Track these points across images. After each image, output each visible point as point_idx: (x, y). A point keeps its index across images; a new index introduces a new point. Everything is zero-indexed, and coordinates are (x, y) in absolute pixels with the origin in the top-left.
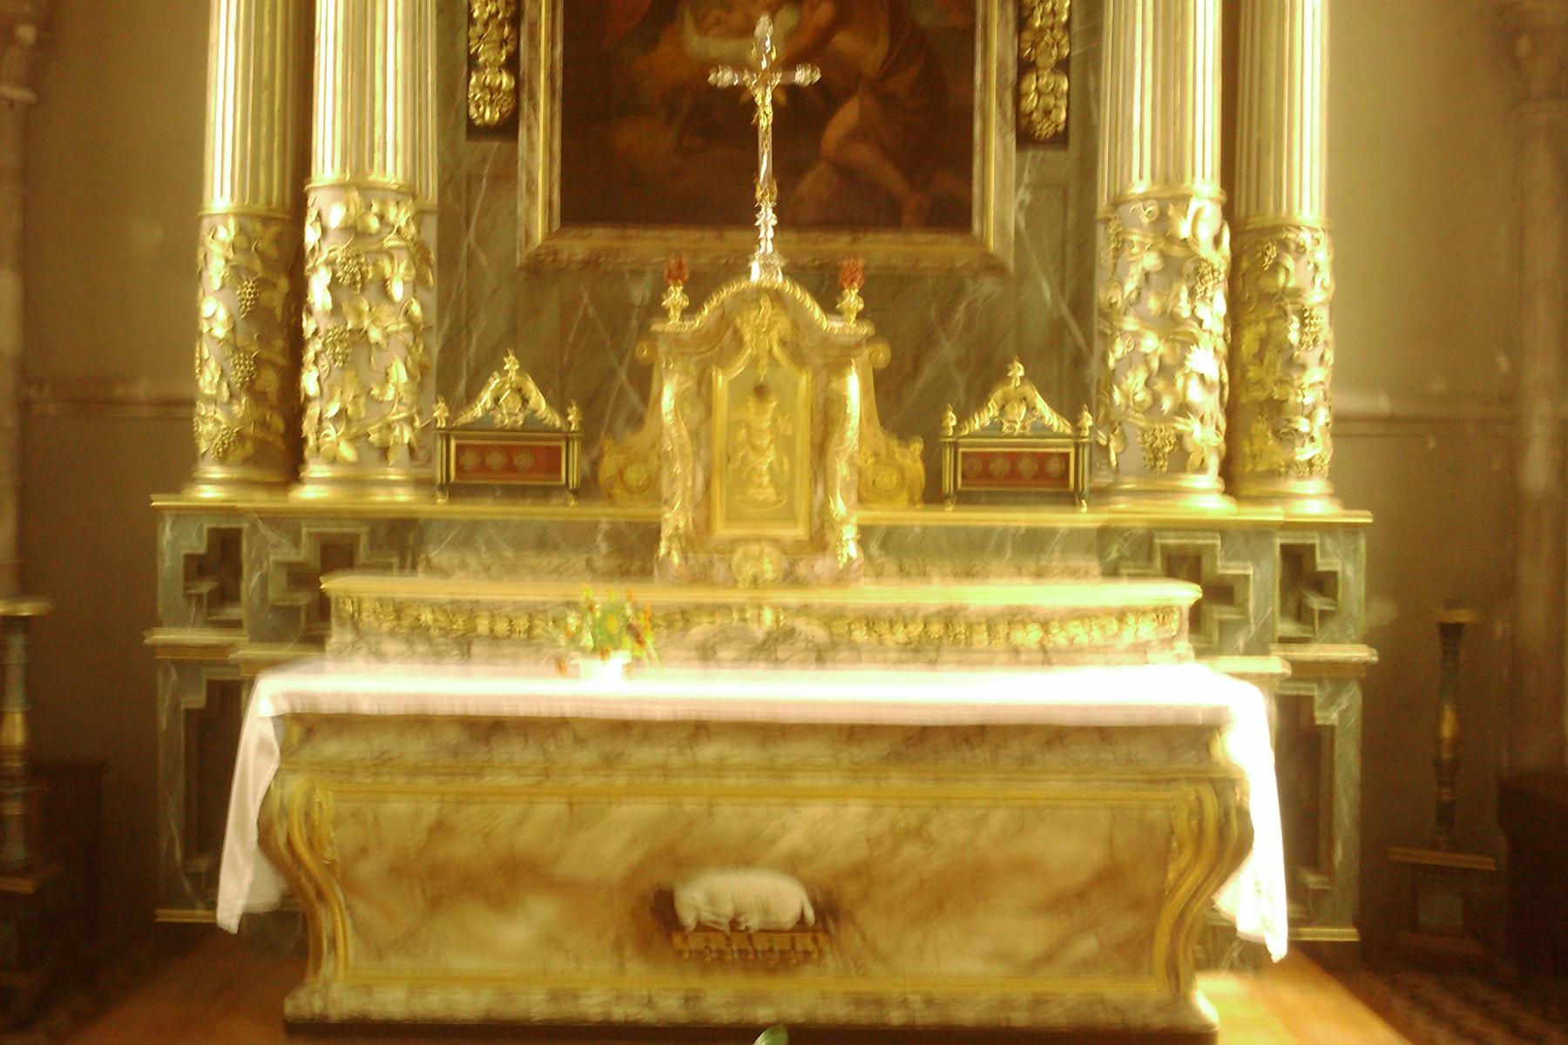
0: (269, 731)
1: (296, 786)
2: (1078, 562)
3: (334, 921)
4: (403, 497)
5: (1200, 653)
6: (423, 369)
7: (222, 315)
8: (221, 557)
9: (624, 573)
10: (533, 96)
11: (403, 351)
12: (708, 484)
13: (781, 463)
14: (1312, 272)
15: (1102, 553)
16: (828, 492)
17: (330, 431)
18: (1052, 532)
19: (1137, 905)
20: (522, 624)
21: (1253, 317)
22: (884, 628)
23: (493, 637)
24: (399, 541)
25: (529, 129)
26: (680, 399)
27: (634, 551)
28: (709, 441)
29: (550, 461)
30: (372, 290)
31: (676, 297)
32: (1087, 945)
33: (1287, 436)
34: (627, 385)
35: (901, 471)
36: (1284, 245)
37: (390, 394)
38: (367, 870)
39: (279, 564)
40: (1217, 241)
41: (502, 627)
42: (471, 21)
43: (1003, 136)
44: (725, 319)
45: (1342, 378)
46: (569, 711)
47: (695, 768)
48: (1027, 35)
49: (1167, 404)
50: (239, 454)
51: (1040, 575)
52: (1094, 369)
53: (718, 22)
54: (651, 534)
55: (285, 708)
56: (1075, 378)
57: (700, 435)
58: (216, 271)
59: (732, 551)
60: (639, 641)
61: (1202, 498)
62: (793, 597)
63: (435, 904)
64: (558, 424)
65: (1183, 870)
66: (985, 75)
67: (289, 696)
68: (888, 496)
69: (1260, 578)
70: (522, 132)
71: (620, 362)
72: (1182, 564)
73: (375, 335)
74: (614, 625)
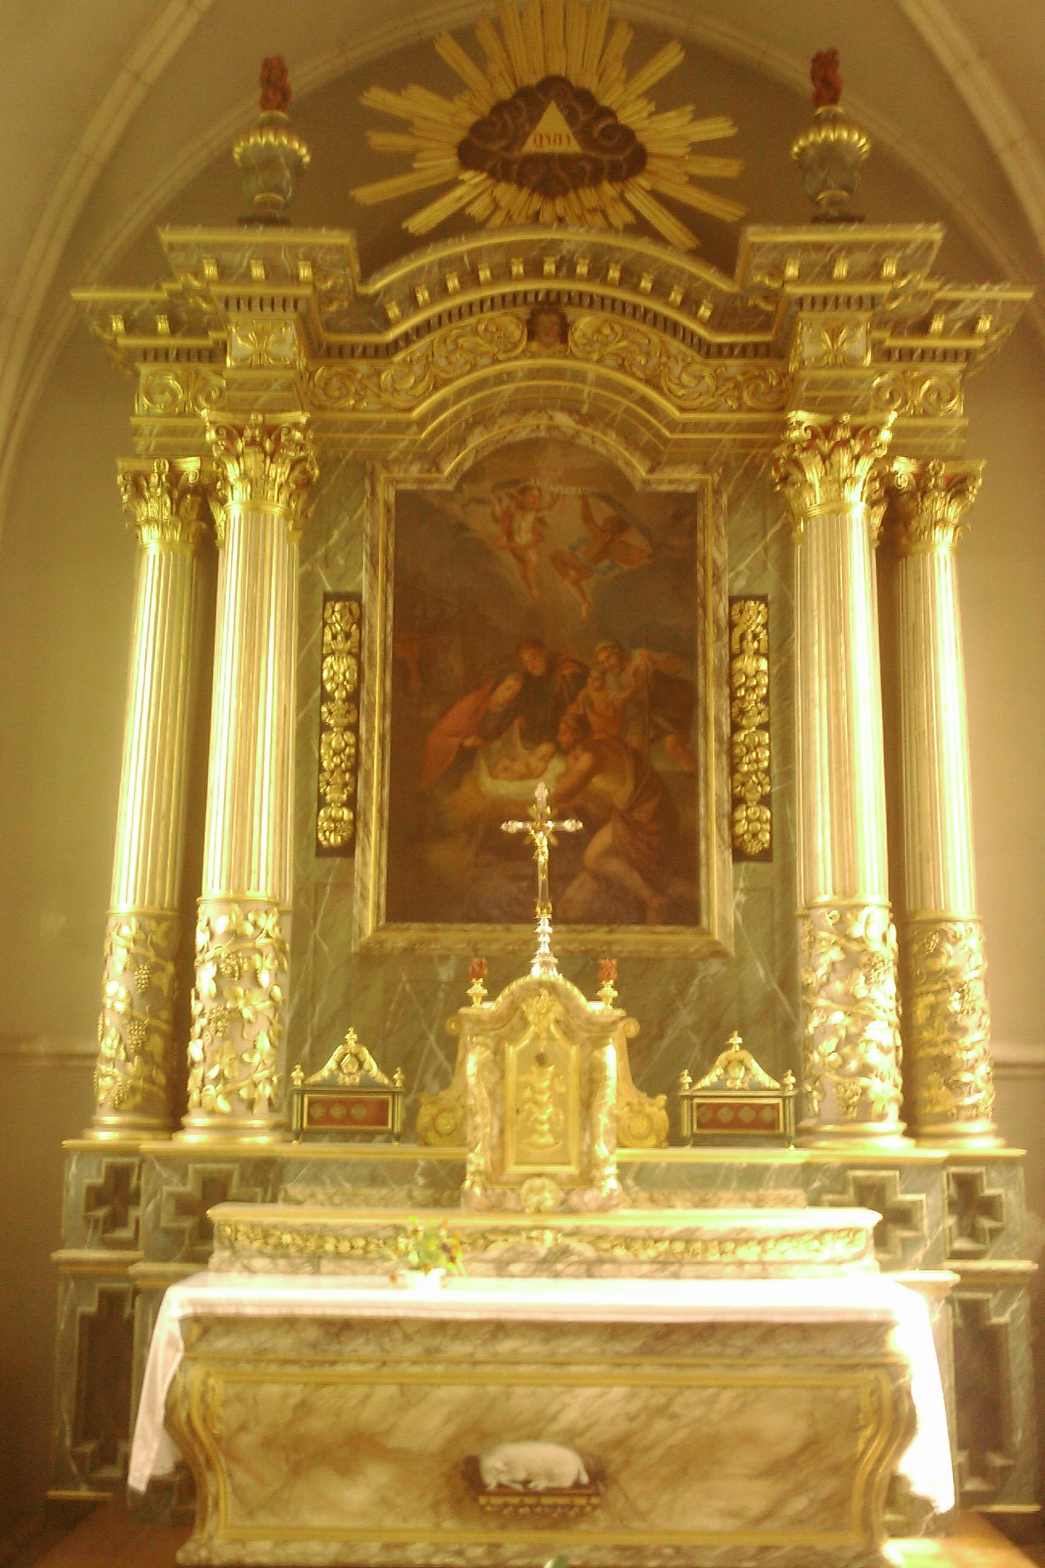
0: (176, 1330)
1: (196, 1373)
2: (791, 1193)
3: (218, 1486)
4: (264, 1141)
5: (885, 1267)
6: (279, 1037)
7: (123, 993)
8: (117, 1190)
9: (436, 1203)
10: (366, 825)
11: (267, 1024)
12: (502, 1131)
13: (557, 1115)
14: (967, 954)
15: (806, 1185)
16: (594, 1139)
17: (211, 1090)
18: (767, 1168)
19: (836, 1469)
20: (361, 1243)
21: (924, 988)
22: (637, 1245)
23: (338, 1255)
24: (264, 1177)
25: (363, 849)
26: (482, 1066)
27: (445, 1185)
28: (503, 1098)
29: (380, 1114)
30: (246, 980)
31: (477, 989)
32: (798, 1504)
33: (955, 1087)
34: (435, 1046)
35: (649, 1117)
36: (943, 934)
37: (257, 1059)
38: (245, 1440)
39: (171, 1195)
40: (884, 938)
41: (344, 1247)
42: (321, 769)
43: (722, 852)
44: (514, 1006)
45: (998, 1033)
46: (401, 1313)
47: (496, 1360)
48: (738, 776)
49: (853, 1066)
50: (130, 1104)
51: (758, 1203)
52: (798, 1034)
53: (506, 769)
54: (457, 1172)
55: (189, 1311)
56: (785, 1050)
57: (496, 1095)
58: (118, 958)
59: (521, 1183)
60: (452, 1259)
61: (887, 1141)
62: (568, 1222)
63: (297, 1470)
64: (386, 1081)
65: (868, 1444)
66: (707, 807)
67: (193, 1303)
68: (639, 1139)
69: (931, 1205)
70: (358, 851)
71: (430, 1027)
72: (869, 1194)
73: (247, 1013)
74: (433, 1246)
